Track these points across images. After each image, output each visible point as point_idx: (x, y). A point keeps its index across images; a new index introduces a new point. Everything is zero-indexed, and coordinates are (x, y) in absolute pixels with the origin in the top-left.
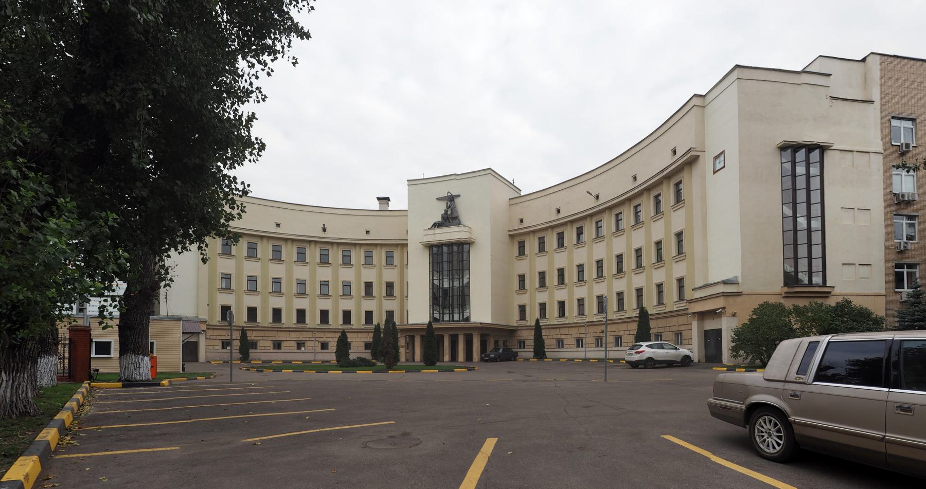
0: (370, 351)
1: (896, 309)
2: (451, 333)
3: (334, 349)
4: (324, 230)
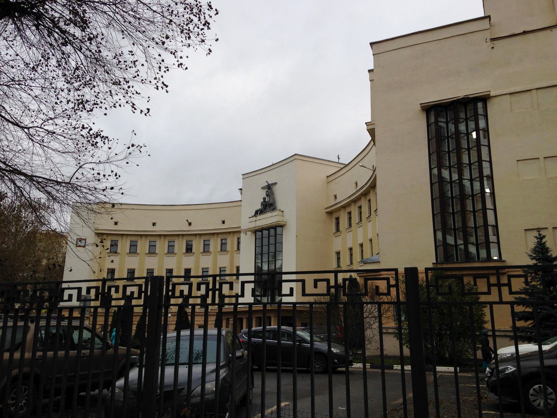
0: (217, 328)
3: (195, 326)
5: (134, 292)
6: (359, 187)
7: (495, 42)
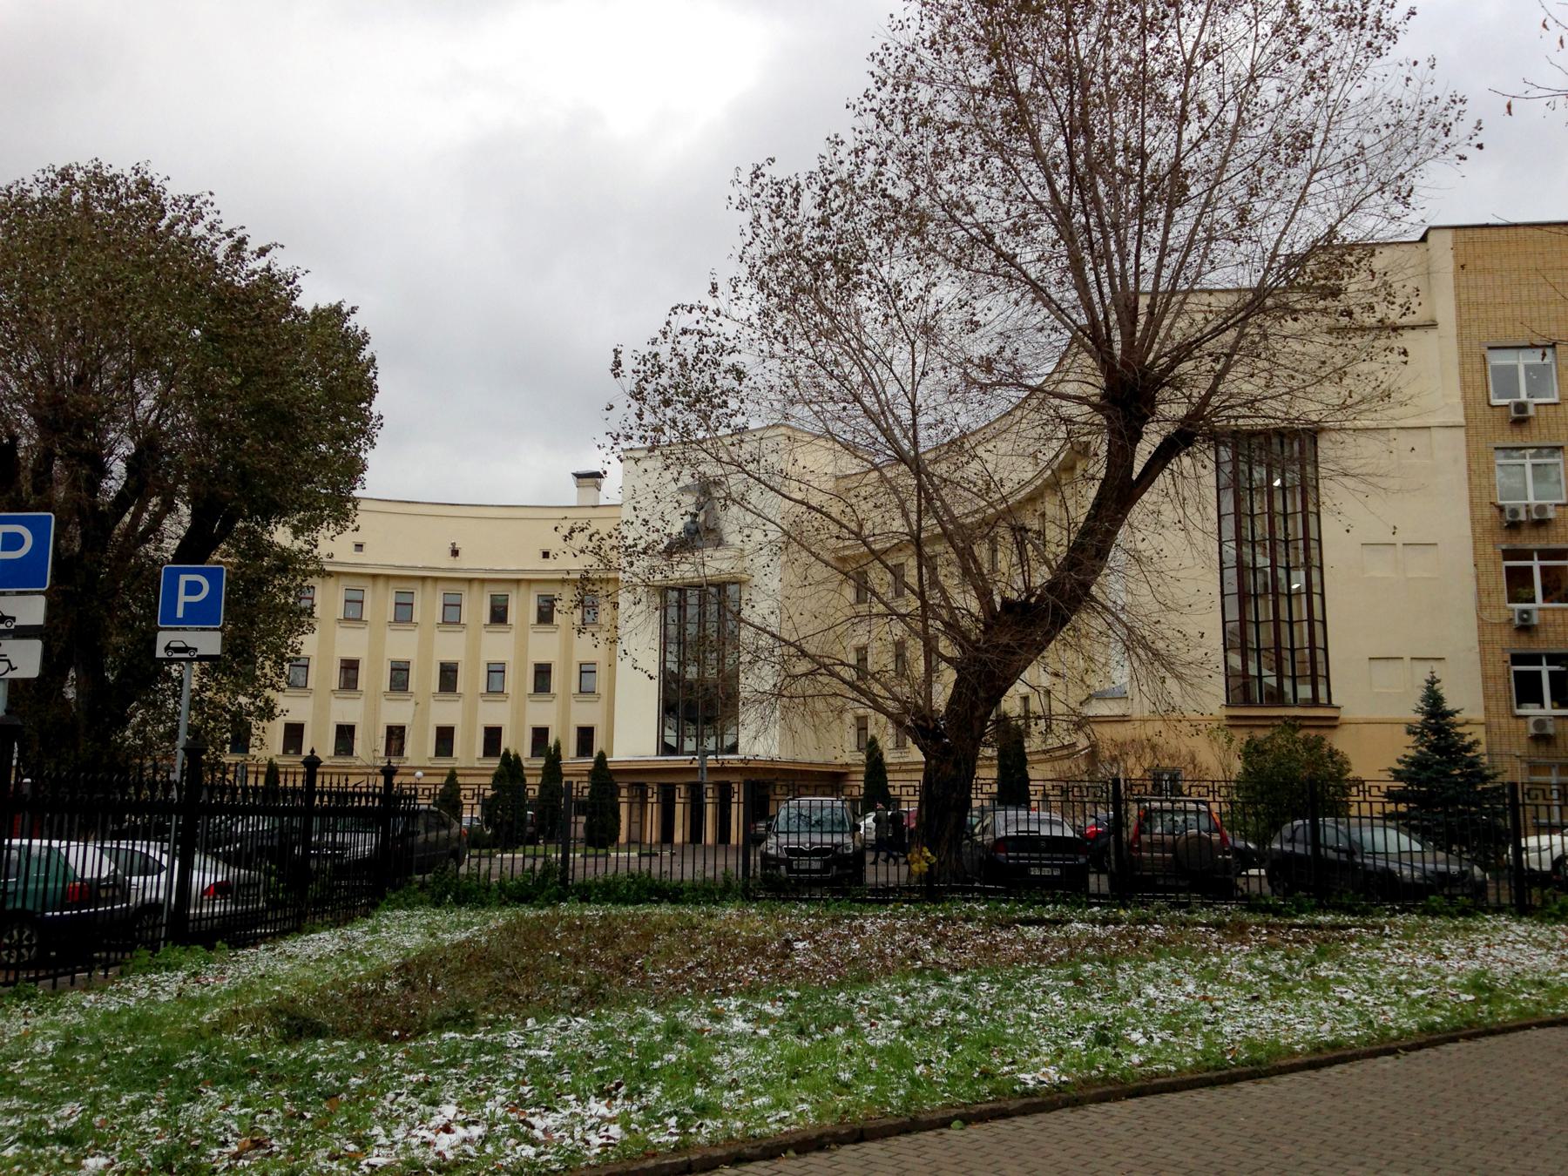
2: (662, 781)
4: (455, 553)
5: (452, 728)
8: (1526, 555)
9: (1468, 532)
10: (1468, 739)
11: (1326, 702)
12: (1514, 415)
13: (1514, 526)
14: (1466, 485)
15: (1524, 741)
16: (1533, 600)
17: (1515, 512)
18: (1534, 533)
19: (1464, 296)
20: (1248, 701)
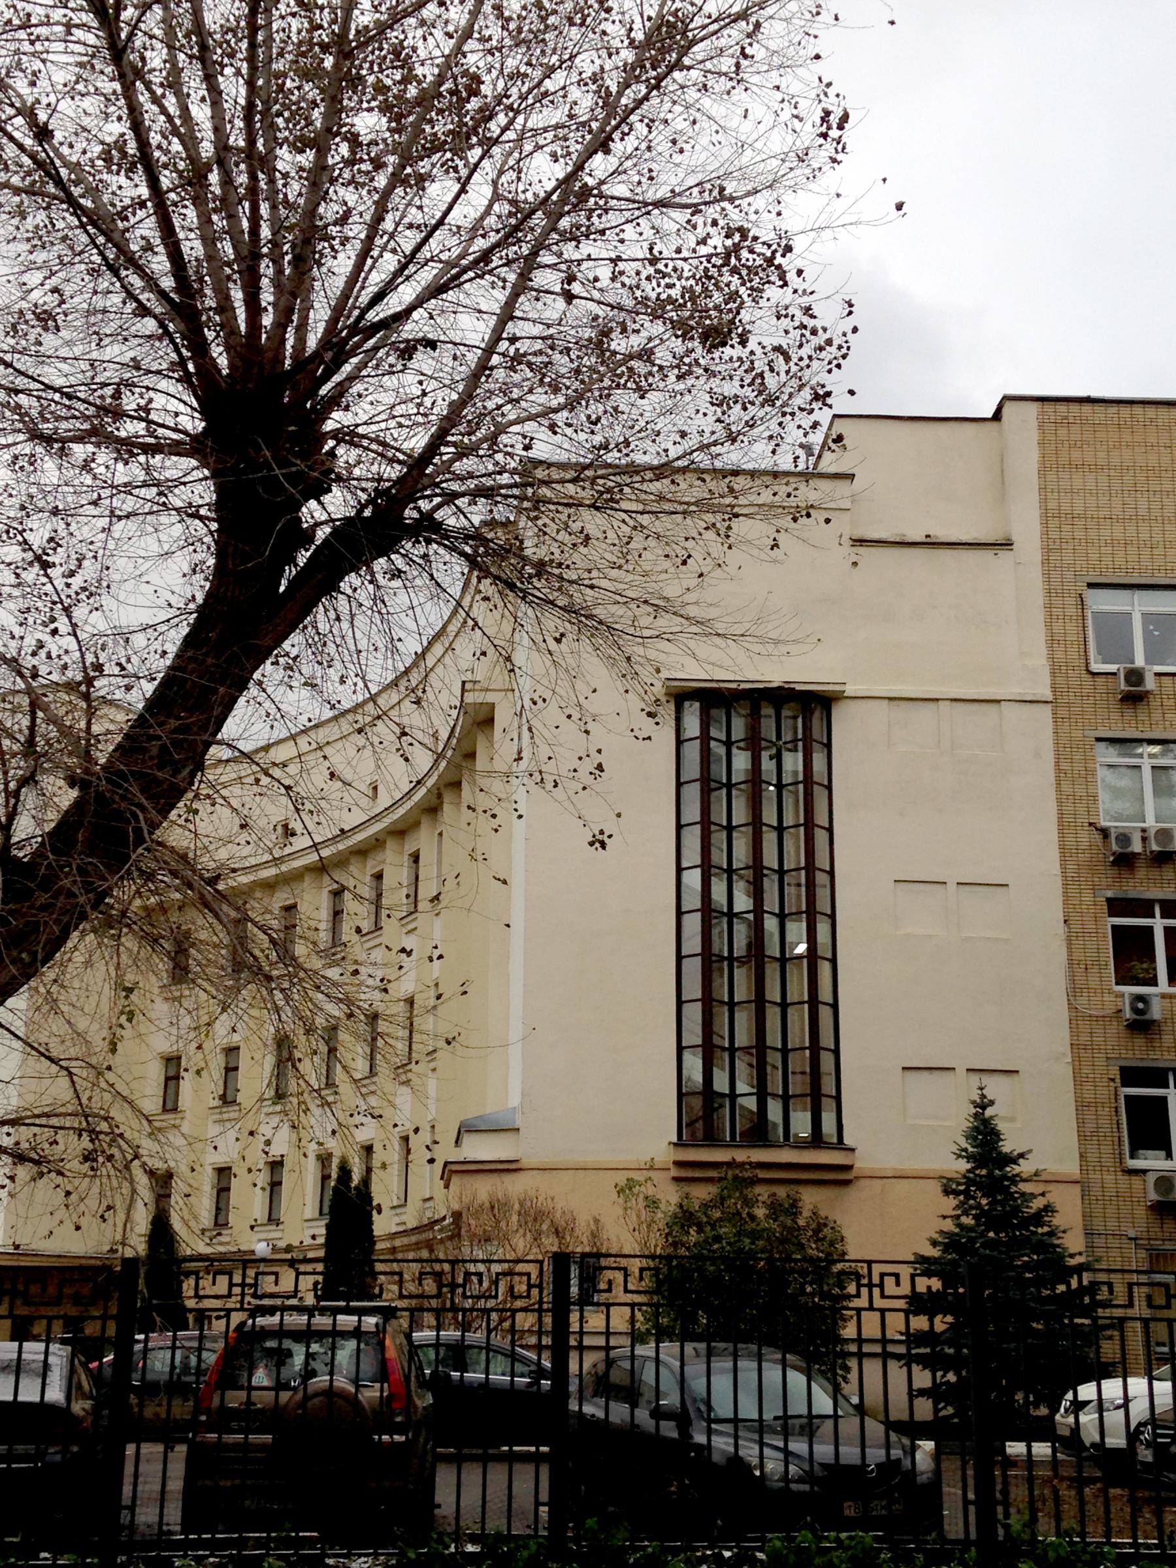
1: (1132, 1234)
6: (384, 801)
7: (862, 550)
8: (1144, 908)
9: (1056, 869)
10: (1038, 1204)
11: (835, 1140)
12: (1123, 686)
13: (1124, 861)
14: (1052, 794)
15: (1141, 1212)
16: (1154, 982)
17: (1124, 839)
18: (1155, 873)
19: (1052, 505)
20: (711, 1139)
